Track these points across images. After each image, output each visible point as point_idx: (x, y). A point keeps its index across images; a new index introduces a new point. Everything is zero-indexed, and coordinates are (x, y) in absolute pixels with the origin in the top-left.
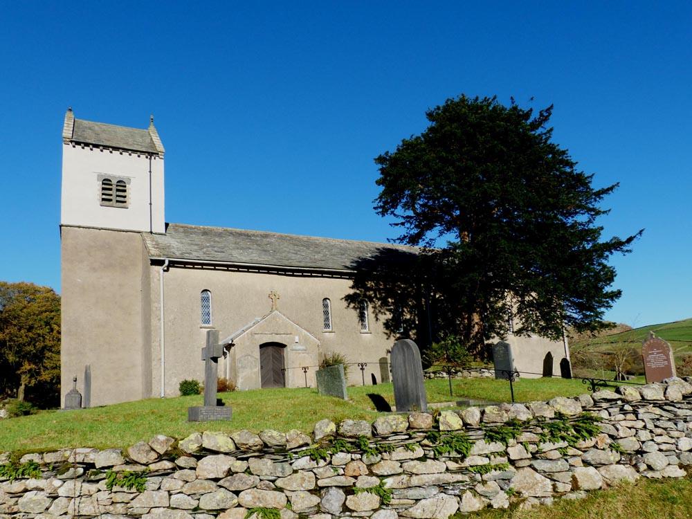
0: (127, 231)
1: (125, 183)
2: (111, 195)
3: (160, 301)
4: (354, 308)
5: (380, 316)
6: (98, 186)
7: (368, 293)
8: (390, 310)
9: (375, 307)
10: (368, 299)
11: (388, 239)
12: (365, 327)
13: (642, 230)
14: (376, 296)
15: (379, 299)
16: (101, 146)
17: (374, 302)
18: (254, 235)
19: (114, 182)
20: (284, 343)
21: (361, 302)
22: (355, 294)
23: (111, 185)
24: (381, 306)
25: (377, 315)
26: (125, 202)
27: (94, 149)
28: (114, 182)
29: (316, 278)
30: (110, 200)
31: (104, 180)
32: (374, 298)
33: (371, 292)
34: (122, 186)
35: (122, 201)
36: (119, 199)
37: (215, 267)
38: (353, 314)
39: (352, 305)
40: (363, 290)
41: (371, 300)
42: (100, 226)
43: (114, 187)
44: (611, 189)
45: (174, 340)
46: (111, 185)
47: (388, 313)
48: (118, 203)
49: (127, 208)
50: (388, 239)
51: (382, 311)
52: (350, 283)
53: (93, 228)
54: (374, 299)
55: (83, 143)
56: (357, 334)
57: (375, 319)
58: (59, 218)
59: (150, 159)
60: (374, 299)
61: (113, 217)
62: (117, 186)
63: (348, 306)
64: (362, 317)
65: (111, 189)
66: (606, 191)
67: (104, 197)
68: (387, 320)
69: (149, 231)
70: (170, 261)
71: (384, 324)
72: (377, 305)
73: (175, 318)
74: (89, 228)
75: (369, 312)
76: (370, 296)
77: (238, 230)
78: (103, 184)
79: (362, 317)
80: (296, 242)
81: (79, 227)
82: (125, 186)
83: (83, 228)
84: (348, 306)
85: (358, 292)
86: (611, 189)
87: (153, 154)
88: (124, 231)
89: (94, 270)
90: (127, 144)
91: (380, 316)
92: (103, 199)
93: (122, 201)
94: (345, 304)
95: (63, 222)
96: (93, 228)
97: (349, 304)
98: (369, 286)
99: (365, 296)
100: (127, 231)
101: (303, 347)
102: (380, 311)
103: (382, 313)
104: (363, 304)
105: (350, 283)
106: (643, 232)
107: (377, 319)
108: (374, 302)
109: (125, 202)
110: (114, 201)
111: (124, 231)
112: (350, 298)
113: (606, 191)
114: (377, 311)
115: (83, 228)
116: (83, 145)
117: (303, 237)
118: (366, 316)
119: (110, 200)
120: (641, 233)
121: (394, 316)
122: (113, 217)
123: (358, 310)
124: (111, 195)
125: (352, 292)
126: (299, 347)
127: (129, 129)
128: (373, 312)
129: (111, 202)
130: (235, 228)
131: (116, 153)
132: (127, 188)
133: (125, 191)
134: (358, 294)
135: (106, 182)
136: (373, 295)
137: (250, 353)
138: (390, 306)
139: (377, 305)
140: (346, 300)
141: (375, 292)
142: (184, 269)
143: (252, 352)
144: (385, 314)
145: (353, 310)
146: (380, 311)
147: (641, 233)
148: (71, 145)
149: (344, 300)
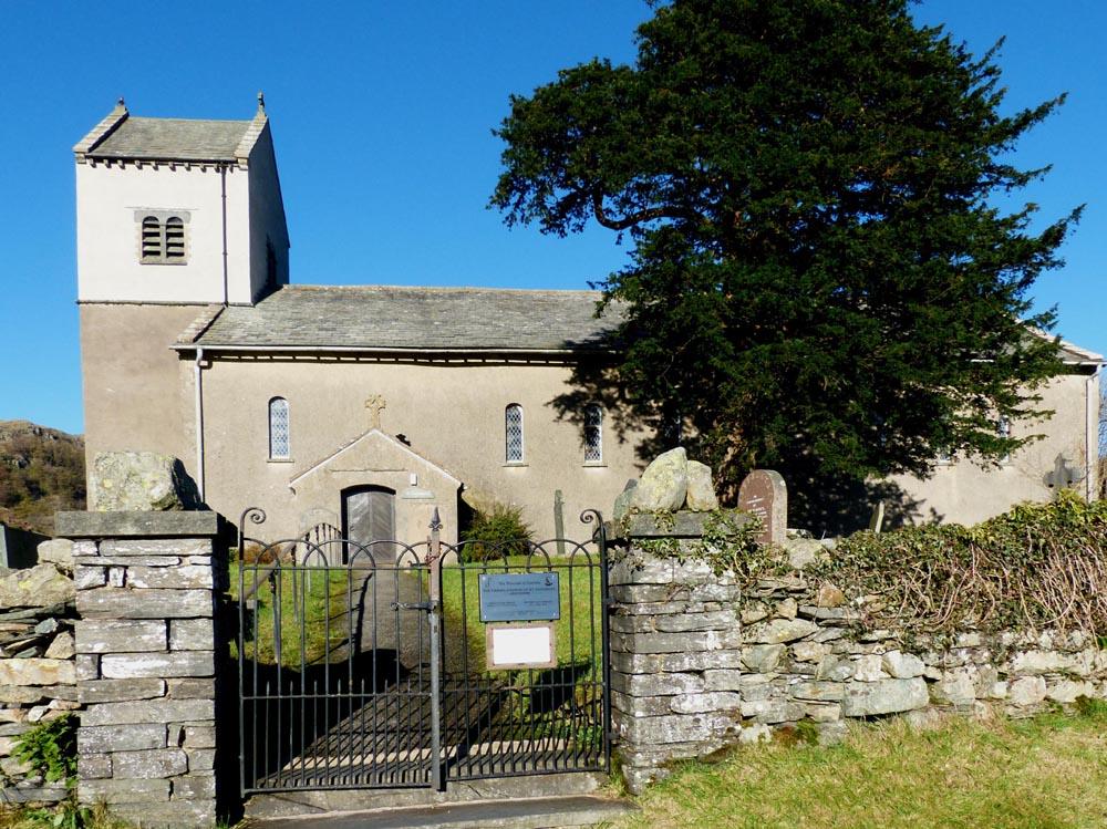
0: (184, 305)
1: (180, 220)
2: (158, 244)
3: (195, 419)
4: (573, 420)
5: (629, 434)
6: (136, 230)
7: (604, 392)
8: (653, 424)
9: (618, 418)
10: (605, 401)
11: (590, 284)
12: (597, 455)
13: (1079, 209)
14: (622, 396)
15: (628, 402)
16: (152, 159)
17: (617, 408)
18: (435, 296)
19: (163, 221)
20: (392, 488)
21: (592, 407)
22: (577, 394)
23: (157, 226)
24: (631, 416)
25: (622, 431)
26: (182, 254)
27: (126, 165)
28: (163, 221)
29: (493, 368)
30: (158, 253)
31: (147, 219)
32: (617, 399)
33: (612, 390)
34: (175, 227)
35: (176, 253)
36: (172, 249)
37: (294, 356)
38: (571, 432)
39: (569, 415)
40: (595, 386)
41: (611, 404)
42: (140, 299)
43: (162, 230)
44: (1043, 111)
45: (222, 483)
46: (157, 226)
47: (647, 428)
48: (171, 258)
49: (185, 264)
50: (590, 284)
51: (634, 424)
52: (568, 373)
53: (129, 303)
54: (618, 403)
55: (106, 158)
56: (574, 468)
57: (618, 440)
58: (76, 291)
59: (224, 173)
60: (618, 403)
61: (163, 281)
62: (168, 227)
63: (560, 418)
64: (590, 436)
65: (157, 234)
66: (1026, 120)
67: (148, 248)
68: (644, 441)
69: (223, 301)
70: (205, 351)
71: (638, 449)
72: (624, 414)
73: (223, 447)
74: (123, 303)
75: (606, 427)
76: (610, 396)
77: (409, 288)
78: (145, 226)
79: (590, 436)
80: (505, 303)
81: (107, 303)
82: (181, 227)
83: (114, 303)
84: (560, 418)
85: (583, 389)
86: (1043, 111)
87: (226, 162)
88: (180, 305)
89: (133, 372)
90: (189, 151)
91: (629, 434)
92: (146, 253)
93: (176, 253)
94: (553, 413)
95: (81, 298)
96: (129, 303)
97: (562, 413)
98: (608, 377)
99: (598, 396)
100: (184, 305)
101: (428, 494)
102: (629, 425)
103: (633, 429)
104: (595, 411)
105: (568, 373)
106: (1083, 213)
107: (622, 440)
108: (617, 408)
109: (182, 254)
110: (163, 254)
111: (180, 305)
112: (564, 403)
113: (1026, 120)
114: (624, 425)
115: (114, 303)
116: (120, 162)
117: (537, 293)
118: (600, 435)
119: (158, 253)
120: (1076, 213)
121: (660, 434)
122: (163, 281)
123: (581, 425)
124: (158, 244)
125: (569, 390)
126: (416, 493)
127: (213, 124)
128: (615, 428)
129: (158, 258)
130: (404, 285)
131: (196, 170)
132: (184, 230)
133: (181, 235)
134: (584, 394)
135: (149, 223)
136: (616, 396)
137: (323, 504)
138: (653, 414)
139: (624, 414)
140: (556, 406)
141: (621, 387)
142: (396, 366)
143: (326, 502)
144: (641, 430)
145: (570, 425)
146: (629, 425)
147: (1076, 213)
148: (89, 162)
149: (551, 406)
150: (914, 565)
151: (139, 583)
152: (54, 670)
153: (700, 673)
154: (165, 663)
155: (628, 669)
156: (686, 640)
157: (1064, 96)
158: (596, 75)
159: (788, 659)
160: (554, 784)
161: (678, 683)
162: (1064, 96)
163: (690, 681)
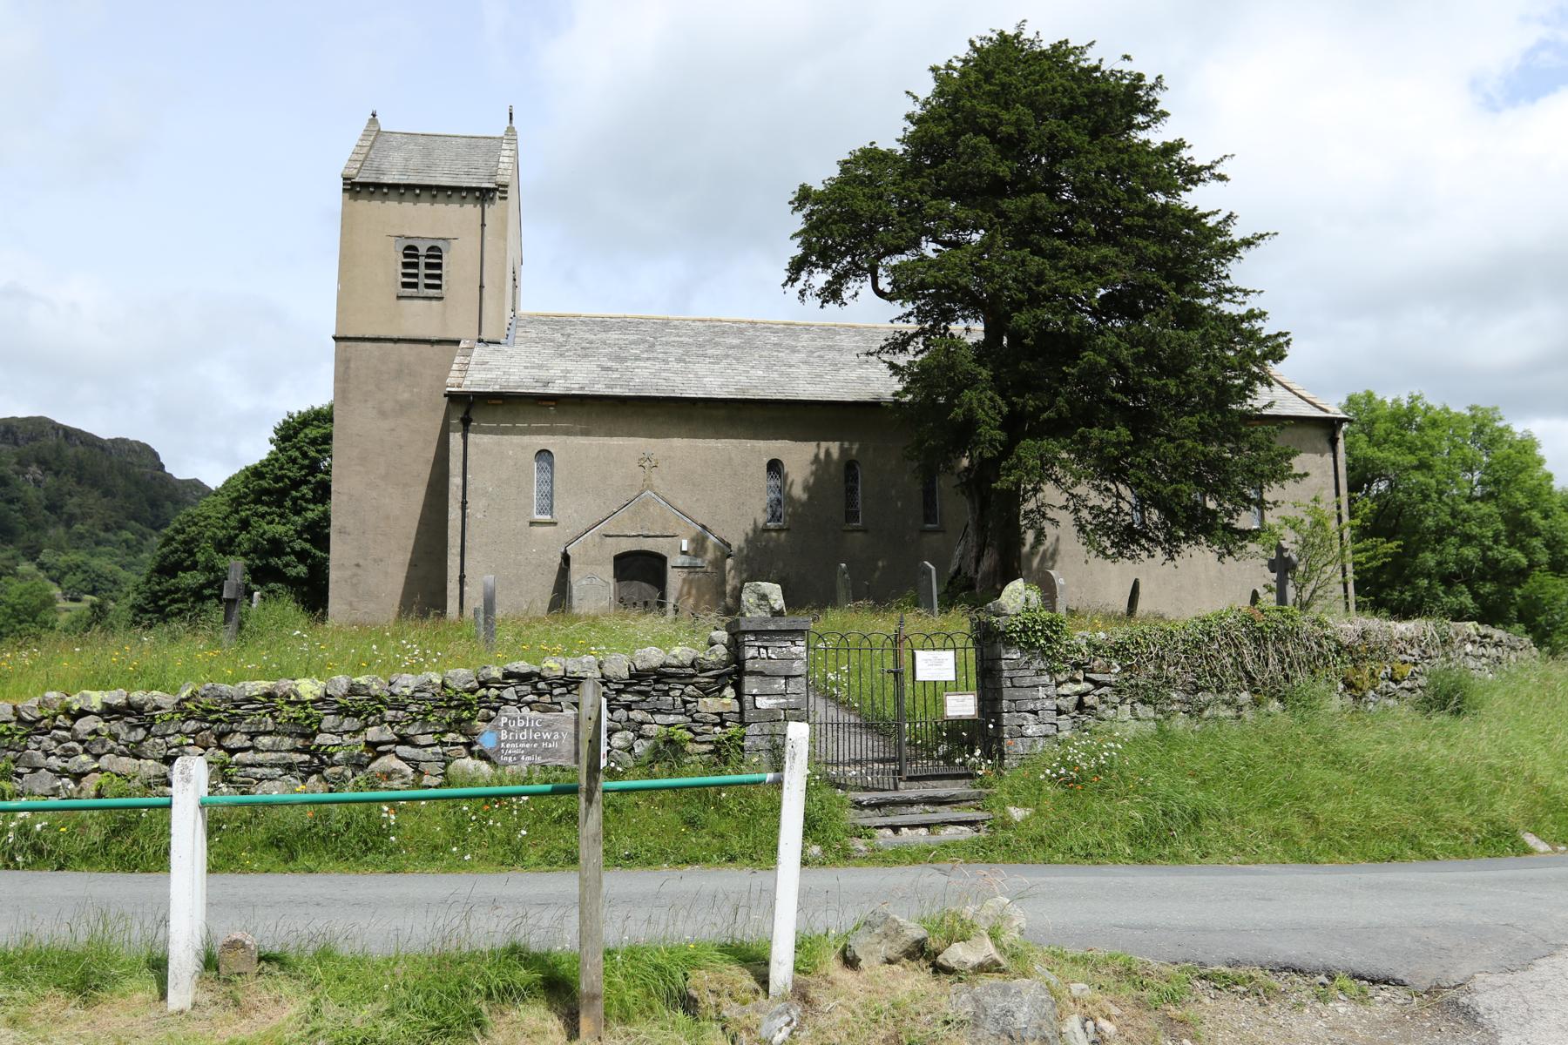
1: (440, 250)
19: (422, 250)
23: (417, 256)
28: (422, 250)
65: (428, 276)
135: (410, 251)
150: (945, 998)
151: (773, 656)
152: (729, 704)
153: (1035, 713)
154: (782, 701)
155: (998, 710)
156: (1028, 693)
157: (1262, 292)
158: (871, 157)
159: (1080, 706)
160: (566, 965)
161: (1025, 719)
162: (1262, 292)
163: (1030, 717)
